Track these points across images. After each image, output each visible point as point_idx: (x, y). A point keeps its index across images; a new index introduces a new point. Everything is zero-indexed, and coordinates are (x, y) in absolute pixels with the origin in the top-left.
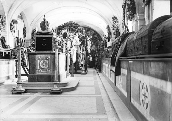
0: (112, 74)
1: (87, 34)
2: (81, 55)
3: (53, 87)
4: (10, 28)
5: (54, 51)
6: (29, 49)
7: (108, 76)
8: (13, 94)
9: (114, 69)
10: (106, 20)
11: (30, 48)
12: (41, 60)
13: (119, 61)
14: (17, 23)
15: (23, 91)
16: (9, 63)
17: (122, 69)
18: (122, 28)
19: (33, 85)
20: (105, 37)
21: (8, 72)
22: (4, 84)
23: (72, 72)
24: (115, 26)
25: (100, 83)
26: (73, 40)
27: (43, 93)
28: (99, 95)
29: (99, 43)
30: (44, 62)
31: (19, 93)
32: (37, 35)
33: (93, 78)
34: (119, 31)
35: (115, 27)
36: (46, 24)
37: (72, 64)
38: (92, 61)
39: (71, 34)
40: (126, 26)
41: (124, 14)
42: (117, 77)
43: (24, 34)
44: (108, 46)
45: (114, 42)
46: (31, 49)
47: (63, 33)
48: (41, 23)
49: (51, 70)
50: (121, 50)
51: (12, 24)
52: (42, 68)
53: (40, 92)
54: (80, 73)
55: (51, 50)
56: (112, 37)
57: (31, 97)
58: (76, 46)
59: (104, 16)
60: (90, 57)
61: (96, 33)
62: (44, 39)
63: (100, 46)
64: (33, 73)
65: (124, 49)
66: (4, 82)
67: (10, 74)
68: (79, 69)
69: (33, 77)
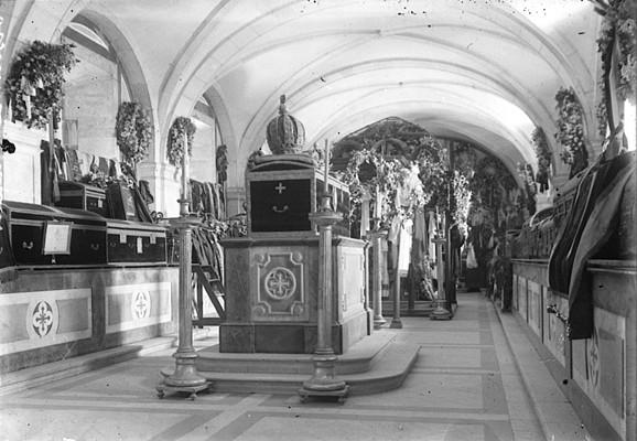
0: (554, 328)
1: (455, 163)
2: (432, 246)
3: (313, 374)
4: (169, 147)
5: (318, 234)
6: (235, 227)
7: (537, 331)
8: (161, 396)
9: (564, 306)
10: (490, 32)
11: (238, 222)
12: (269, 268)
13: (587, 278)
14: (191, 129)
15: (199, 388)
16: (158, 279)
17: (599, 313)
18: (598, 136)
19: (231, 365)
20: (528, 172)
21: (155, 312)
22: (142, 353)
23: (395, 309)
24: (568, 127)
25: (503, 358)
26: (399, 190)
27: (274, 396)
28: (499, 413)
29: (504, 194)
30: (280, 276)
31: (184, 395)
32: (256, 170)
33: (475, 337)
34: (583, 146)
35: (568, 131)
36: (289, 130)
37: (395, 279)
38: (476, 265)
39: (390, 166)
40: (616, 126)
41: (606, 77)
42: (578, 344)
43: (218, 168)
44: (539, 208)
45: (561, 192)
46: (241, 223)
47: (359, 163)
48: (268, 128)
49: (307, 306)
50: (598, 227)
51: (176, 134)
52: (270, 300)
53: (262, 392)
54: (427, 316)
55: (308, 227)
56: (557, 173)
57: (226, 411)
58: (410, 211)
59: (523, 91)
60: (467, 250)
61: (491, 159)
62: (281, 188)
63: (508, 209)
64: (239, 319)
65: (612, 222)
66: (140, 348)
67: (166, 318)
68: (424, 297)
69: (239, 335)
